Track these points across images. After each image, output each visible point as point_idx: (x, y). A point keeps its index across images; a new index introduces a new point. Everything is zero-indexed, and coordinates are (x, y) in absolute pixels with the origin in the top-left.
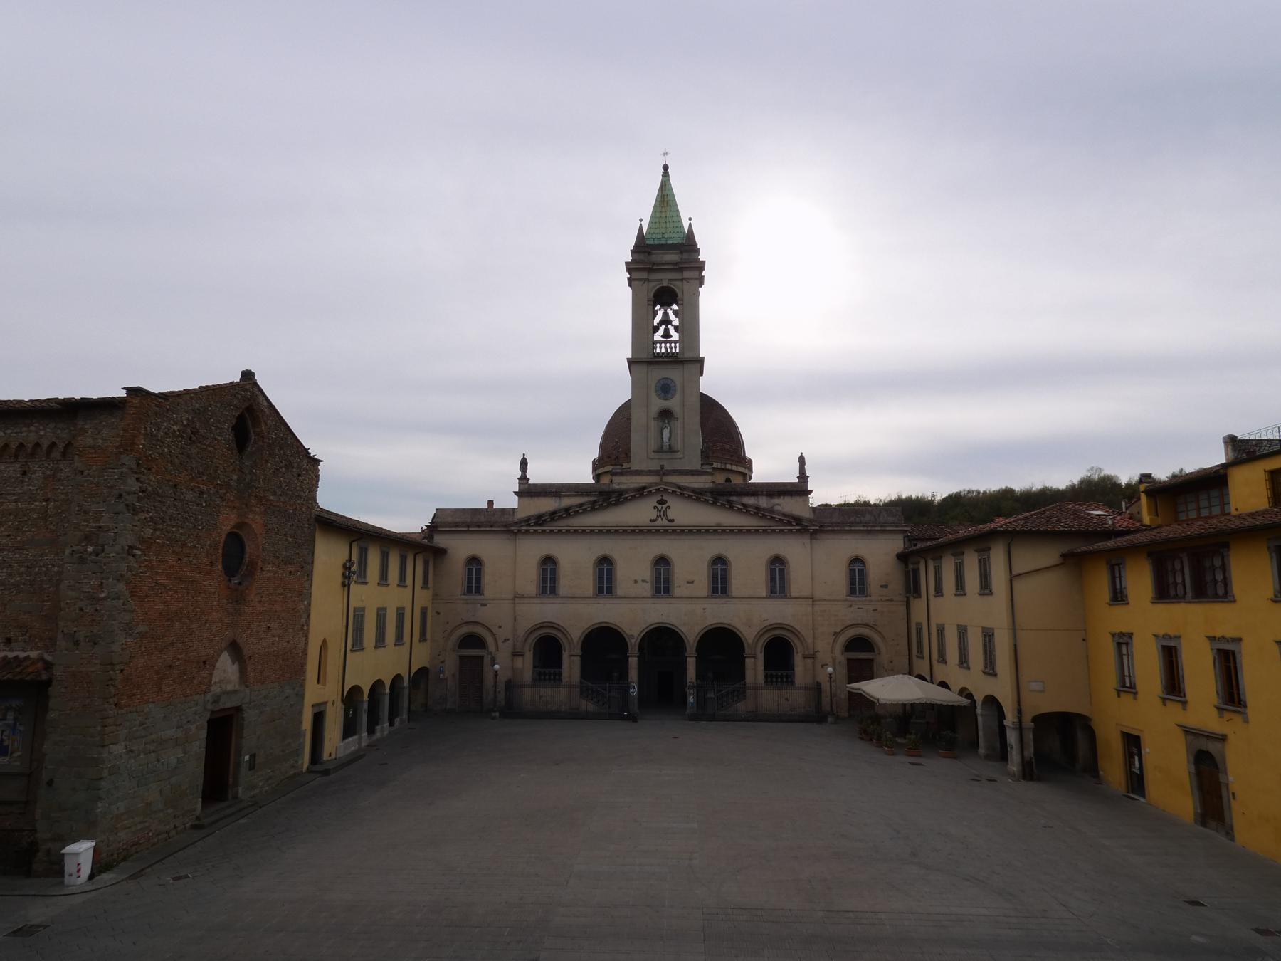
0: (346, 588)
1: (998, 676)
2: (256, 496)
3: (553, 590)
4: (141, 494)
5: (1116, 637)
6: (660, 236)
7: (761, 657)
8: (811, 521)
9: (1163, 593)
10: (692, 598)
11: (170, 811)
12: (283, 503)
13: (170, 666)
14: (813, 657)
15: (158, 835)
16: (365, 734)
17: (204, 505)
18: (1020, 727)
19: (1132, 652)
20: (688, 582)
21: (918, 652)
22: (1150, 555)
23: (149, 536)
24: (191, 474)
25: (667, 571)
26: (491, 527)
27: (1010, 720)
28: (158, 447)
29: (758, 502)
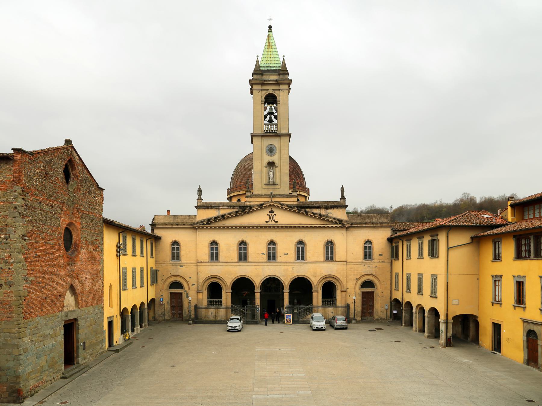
0: (118, 257)
1: (438, 298)
2: (76, 208)
3: (217, 259)
4: (25, 207)
5: (494, 277)
6: (267, 65)
7: (320, 292)
8: (347, 221)
9: (519, 256)
10: (287, 262)
11: (51, 370)
12: (88, 212)
13: (45, 298)
14: (345, 291)
15: (47, 382)
16: (130, 332)
17: (54, 213)
18: (447, 322)
19: (501, 284)
20: (285, 254)
21: (396, 287)
22: (514, 237)
23: (31, 230)
24: (47, 196)
25: (274, 248)
26: (184, 225)
27: (442, 319)
28: (31, 181)
29: (320, 211)
